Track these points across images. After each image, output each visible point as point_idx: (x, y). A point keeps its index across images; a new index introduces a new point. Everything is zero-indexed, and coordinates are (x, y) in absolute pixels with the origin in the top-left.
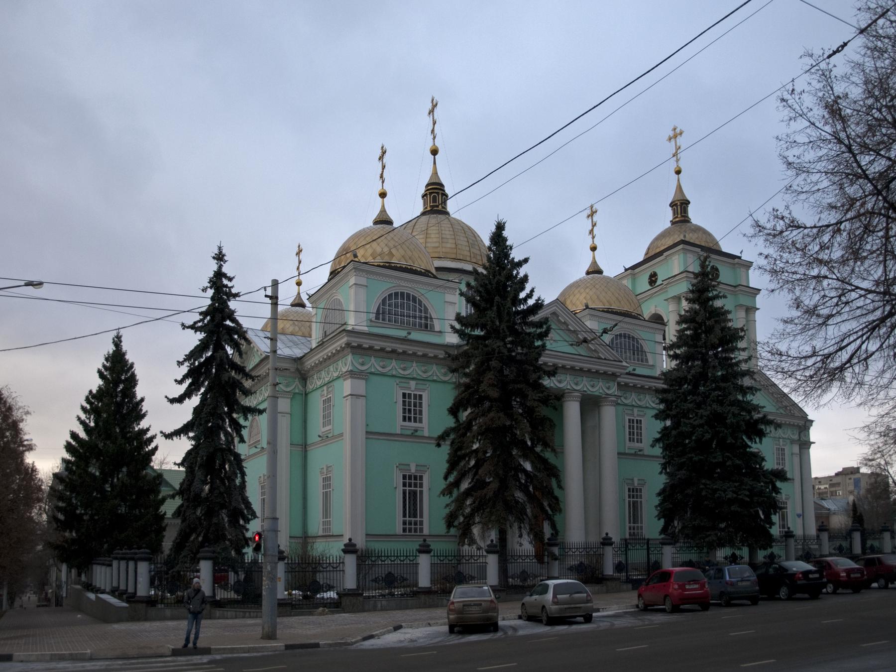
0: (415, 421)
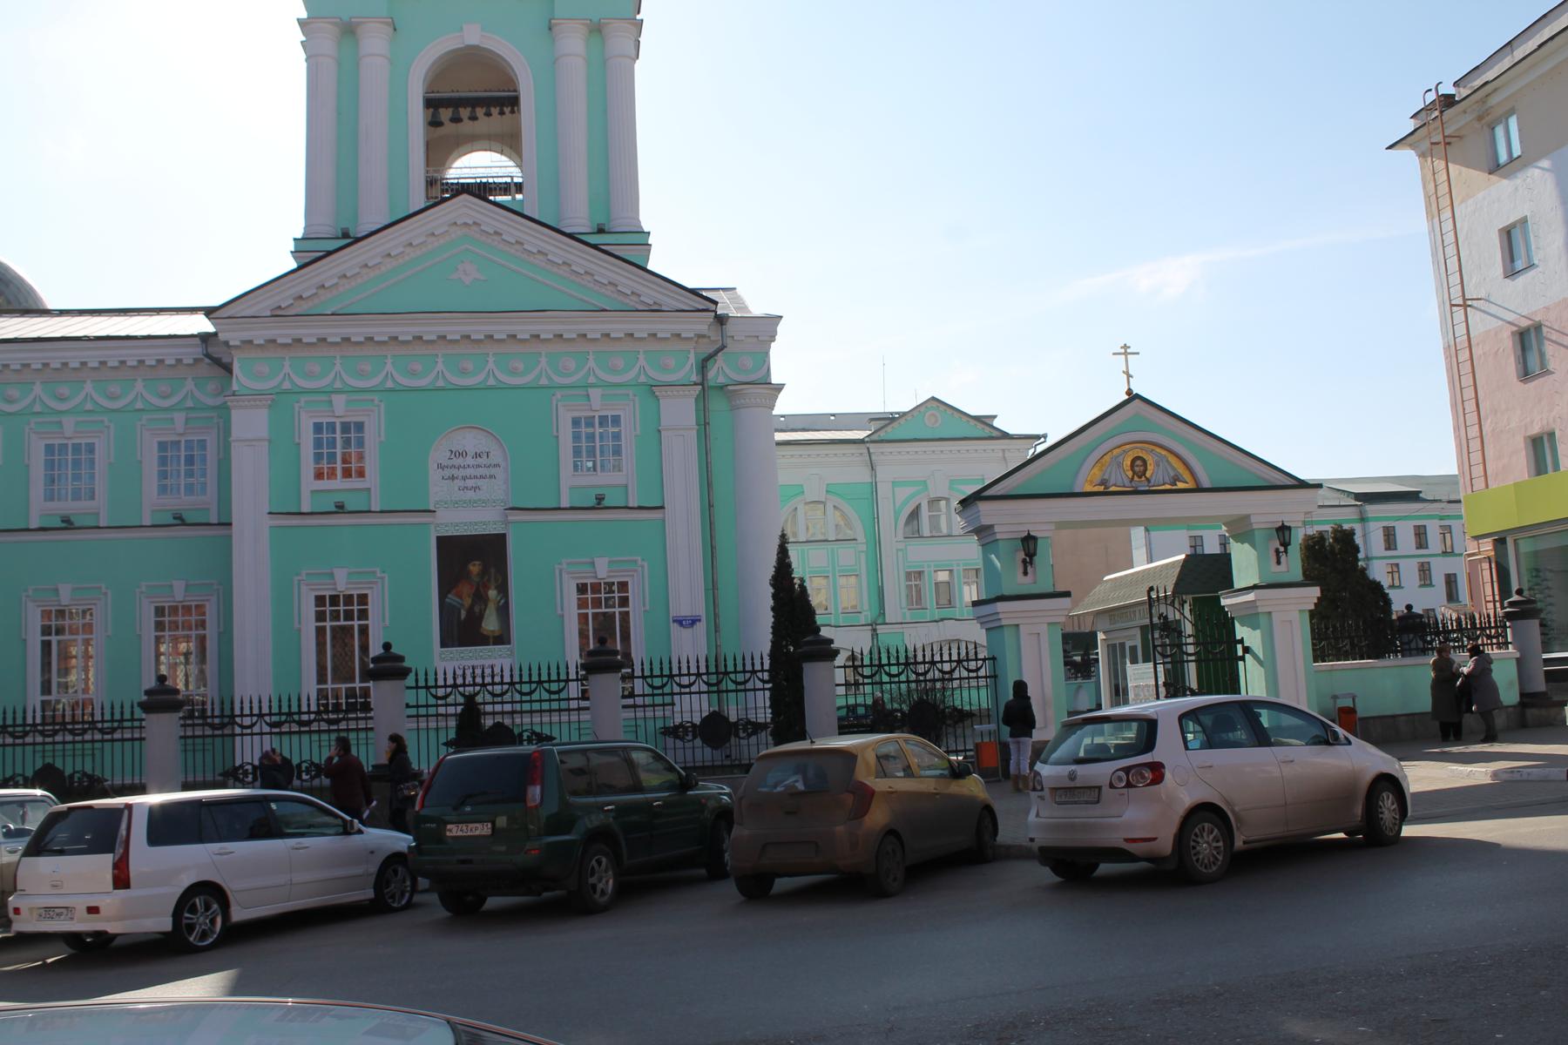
0: (347, 473)
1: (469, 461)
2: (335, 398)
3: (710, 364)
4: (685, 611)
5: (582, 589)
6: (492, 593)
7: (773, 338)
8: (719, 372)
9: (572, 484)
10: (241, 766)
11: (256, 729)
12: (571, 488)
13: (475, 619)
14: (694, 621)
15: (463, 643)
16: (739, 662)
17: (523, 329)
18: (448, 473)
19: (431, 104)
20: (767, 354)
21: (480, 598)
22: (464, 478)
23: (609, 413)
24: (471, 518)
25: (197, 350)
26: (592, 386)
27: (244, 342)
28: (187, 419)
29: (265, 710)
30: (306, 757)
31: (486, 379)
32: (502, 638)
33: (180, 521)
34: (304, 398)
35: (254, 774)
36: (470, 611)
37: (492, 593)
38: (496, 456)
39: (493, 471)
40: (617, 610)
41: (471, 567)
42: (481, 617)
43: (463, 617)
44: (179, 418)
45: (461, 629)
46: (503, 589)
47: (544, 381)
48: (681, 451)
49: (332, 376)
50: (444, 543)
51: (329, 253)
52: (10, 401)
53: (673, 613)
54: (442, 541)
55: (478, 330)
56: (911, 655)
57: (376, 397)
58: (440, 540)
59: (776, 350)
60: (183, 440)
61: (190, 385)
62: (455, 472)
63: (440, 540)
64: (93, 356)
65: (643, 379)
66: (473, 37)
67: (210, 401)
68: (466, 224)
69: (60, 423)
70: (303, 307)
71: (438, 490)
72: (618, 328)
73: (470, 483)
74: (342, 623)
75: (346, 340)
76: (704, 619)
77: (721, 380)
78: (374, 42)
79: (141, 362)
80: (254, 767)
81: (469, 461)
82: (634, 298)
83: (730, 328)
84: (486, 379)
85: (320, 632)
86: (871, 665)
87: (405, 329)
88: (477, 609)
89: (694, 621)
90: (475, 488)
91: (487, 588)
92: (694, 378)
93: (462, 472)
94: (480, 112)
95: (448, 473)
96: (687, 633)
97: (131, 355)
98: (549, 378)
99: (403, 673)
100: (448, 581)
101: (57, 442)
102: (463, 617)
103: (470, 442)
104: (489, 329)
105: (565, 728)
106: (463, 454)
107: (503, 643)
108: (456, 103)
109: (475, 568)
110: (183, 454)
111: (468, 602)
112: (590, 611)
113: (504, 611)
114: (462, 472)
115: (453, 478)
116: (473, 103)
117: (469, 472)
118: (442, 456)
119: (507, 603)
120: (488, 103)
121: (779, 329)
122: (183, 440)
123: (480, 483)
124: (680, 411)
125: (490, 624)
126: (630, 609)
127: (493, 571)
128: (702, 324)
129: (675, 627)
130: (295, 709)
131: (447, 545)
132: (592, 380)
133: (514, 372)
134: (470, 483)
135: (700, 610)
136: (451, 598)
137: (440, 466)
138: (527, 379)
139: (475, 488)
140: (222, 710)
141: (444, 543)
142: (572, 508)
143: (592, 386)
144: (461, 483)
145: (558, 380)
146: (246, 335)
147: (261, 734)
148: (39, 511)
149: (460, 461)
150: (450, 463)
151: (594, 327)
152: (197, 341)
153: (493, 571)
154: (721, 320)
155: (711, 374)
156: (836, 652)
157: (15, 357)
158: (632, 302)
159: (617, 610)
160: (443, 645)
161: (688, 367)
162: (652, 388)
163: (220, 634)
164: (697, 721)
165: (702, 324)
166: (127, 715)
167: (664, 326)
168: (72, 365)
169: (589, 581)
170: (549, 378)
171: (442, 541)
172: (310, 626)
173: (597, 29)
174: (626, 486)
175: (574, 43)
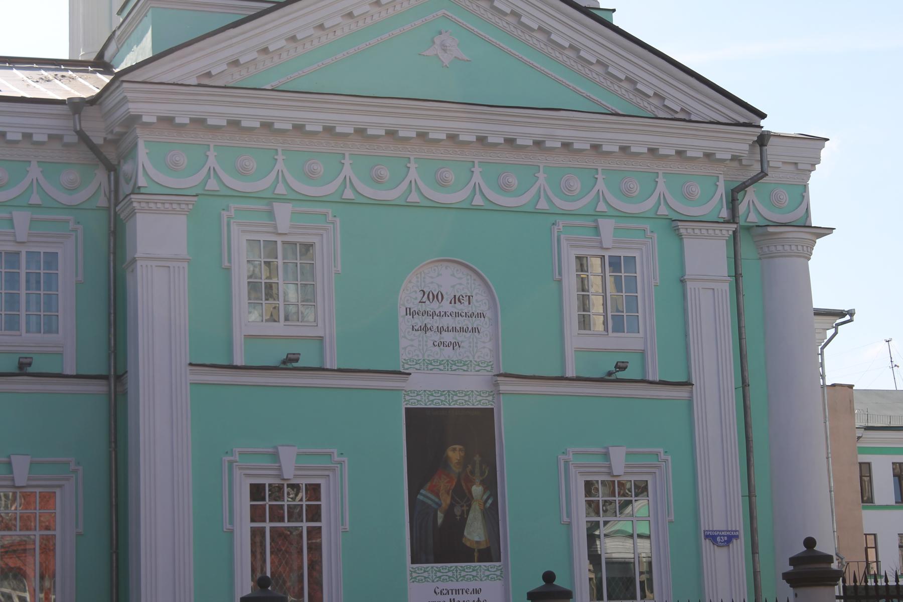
2: (278, 207)
3: (740, 196)
4: (718, 524)
5: (257, 491)
6: (477, 490)
8: (753, 208)
12: (578, 350)
14: (730, 538)
18: (418, 321)
20: (805, 187)
21: (462, 495)
22: (440, 330)
24: (457, 387)
26: (603, 215)
27: (194, 121)
31: (205, 182)
36: (449, 513)
37: (477, 490)
38: (480, 303)
41: (450, 453)
42: (462, 523)
44: (22, 218)
47: (543, 205)
48: (710, 308)
54: (412, 415)
58: (408, 410)
59: (817, 182)
60: (23, 250)
62: (428, 320)
65: (663, 210)
67: (64, 198)
70: (236, 77)
71: (410, 346)
72: (640, 138)
73: (448, 337)
74: (286, 524)
77: (753, 218)
79: (27, 136)
81: (446, 306)
82: (655, 101)
83: (771, 149)
84: (205, 182)
87: (696, 142)
88: (457, 511)
89: (730, 538)
90: (455, 345)
92: (725, 214)
93: (436, 322)
95: (418, 321)
96: (721, 553)
98: (549, 200)
99: (830, 578)
100: (419, 474)
102: (440, 521)
103: (450, 281)
106: (437, 297)
109: (454, 454)
110: (23, 271)
111: (446, 500)
112: (268, 525)
113: (492, 516)
114: (436, 322)
115: (425, 329)
117: (447, 322)
119: (495, 504)
121: (823, 153)
122: (23, 250)
124: (708, 255)
126: (323, 524)
128: (739, 143)
129: (706, 544)
132: (281, 190)
134: (448, 337)
135: (739, 524)
136: (424, 495)
137: (410, 312)
139: (455, 345)
142: (578, 379)
143: (603, 215)
144: (436, 337)
145: (369, 191)
149: (434, 306)
150: (422, 308)
151: (612, 137)
154: (763, 139)
155: (742, 208)
157: (13, 125)
158: (652, 106)
159: (305, 525)
161: (717, 198)
162: (675, 225)
163: (78, 535)
165: (739, 143)
167: (697, 143)
168: (36, 138)
169: (267, 481)
170: (549, 200)
174: (643, 353)
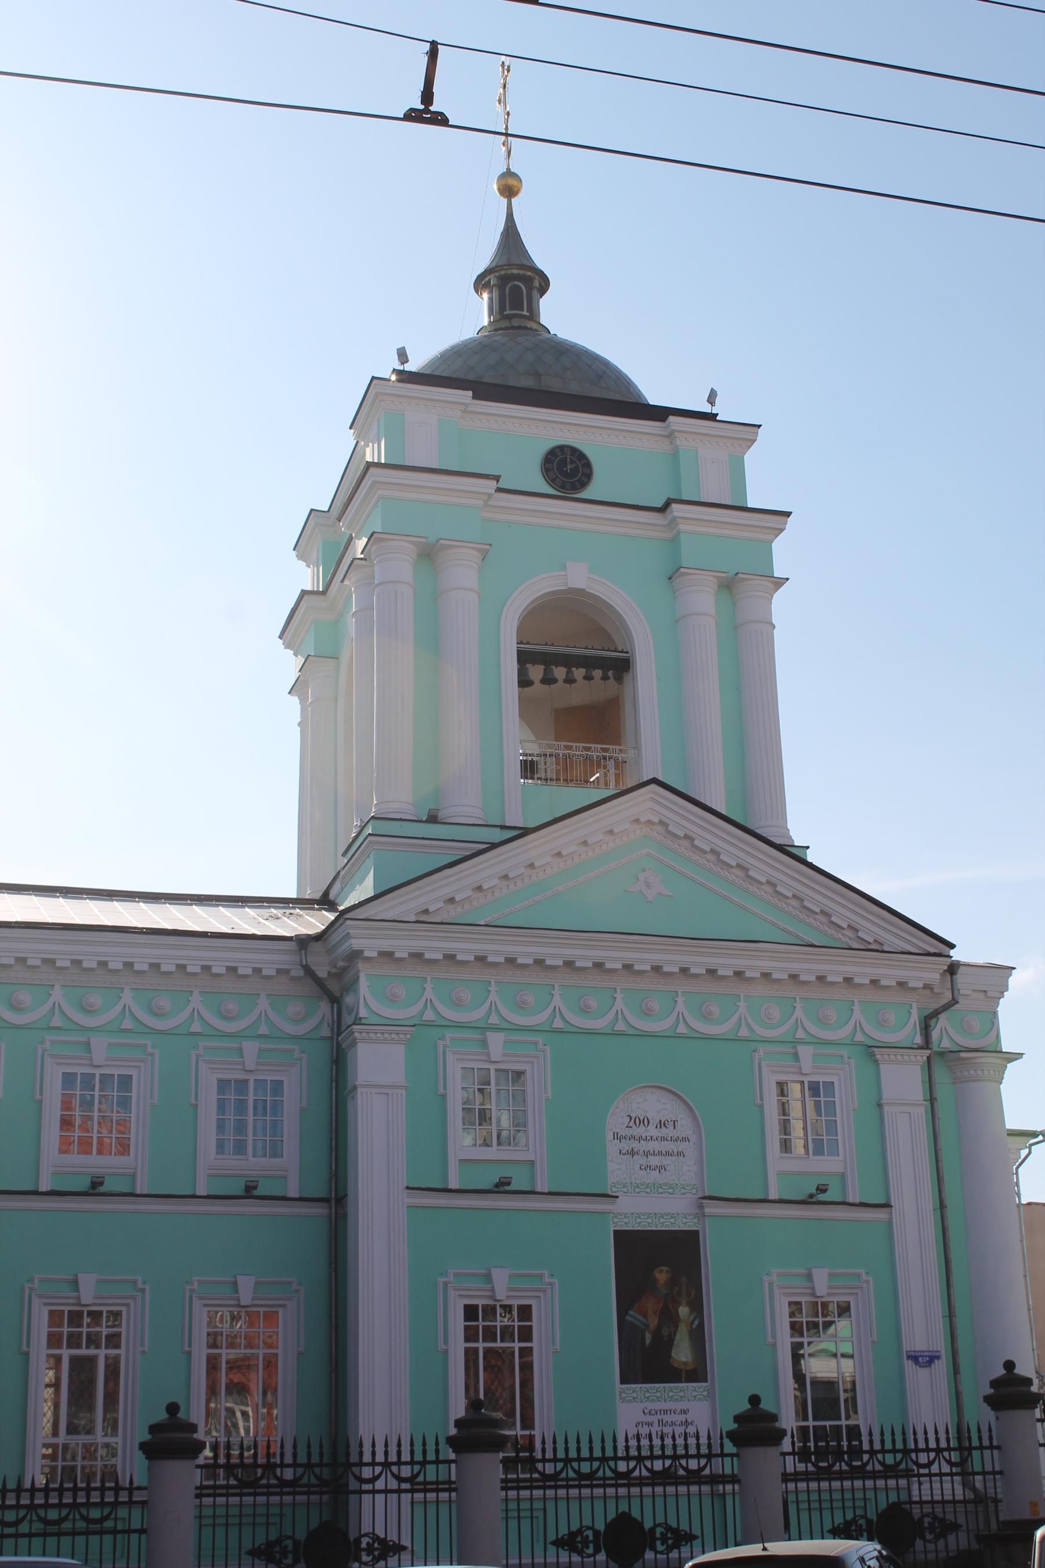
1: (652, 1131)
3: (933, 1022)
4: (920, 1345)
5: (470, 1312)
6: (683, 1311)
7: (1001, 994)
8: (947, 1032)
9: (785, 1170)
10: (580, 1531)
11: (380, 1485)
13: (664, 1344)
14: (932, 1359)
15: (649, 1377)
16: (549, 1446)
17: (726, 963)
18: (626, 1145)
19: (524, 658)
21: (669, 1317)
22: (646, 1154)
23: (821, 1079)
25: (286, 959)
26: (802, 1042)
27: (382, 954)
28: (260, 1050)
29: (393, 1458)
30: (660, 1519)
32: (697, 1373)
33: (249, 1192)
34: (450, 1033)
35: (654, 1539)
36: (657, 1334)
37: (683, 1311)
38: (685, 1127)
39: (682, 1146)
40: (517, 1345)
41: (658, 1275)
42: (670, 1343)
43: (648, 1341)
44: (251, 1048)
45: (648, 1360)
46: (697, 1305)
49: (611, 1015)
50: (624, 1240)
51: (494, 846)
52: (16, 1007)
53: (907, 1346)
54: (621, 1237)
55: (672, 960)
56: (276, 1449)
57: (540, 1039)
58: (615, 1232)
60: (252, 1078)
61: (263, 1004)
62: (635, 1145)
63: (615, 1232)
64: (142, 955)
65: (859, 1037)
66: (578, 578)
67: (290, 1028)
68: (649, 822)
69: (88, 1044)
70: (452, 913)
71: (618, 1170)
72: (836, 968)
73: (654, 1161)
74: (498, 1344)
75: (450, 958)
76: (943, 1356)
77: (946, 1044)
78: (463, 573)
80: (296, 1543)
81: (652, 1131)
83: (960, 977)
85: (470, 1355)
86: (294, 1465)
88: (665, 1332)
89: (932, 1359)
90: (661, 1168)
91: (678, 1304)
93: (643, 1146)
94: (579, 673)
95: (626, 1145)
96: (923, 1373)
97: (194, 957)
100: (629, 1293)
101: (80, 1070)
102: (648, 1341)
104: (685, 959)
105: (648, 1503)
106: (644, 1122)
107: (697, 1380)
108: (548, 660)
109: (662, 1276)
111: (653, 1321)
112: (481, 1345)
113: (698, 1337)
114: (643, 1146)
115: (632, 1153)
116: (569, 661)
118: (617, 1122)
119: (701, 1325)
120: (589, 663)
123: (666, 1161)
124: (903, 1080)
125: (682, 1353)
127: (684, 1279)
128: (931, 972)
129: (909, 1364)
130: (393, 1458)
131: (628, 1243)
132: (494, 1019)
133: (457, 1003)
134: (654, 1161)
135: (941, 1345)
136: (632, 1315)
137: (617, 1136)
138: (540, 1019)
139: (661, 1168)
140: (295, 1455)
141: (624, 1240)
143: (802, 1042)
146: (385, 945)
147: (386, 1491)
148: (55, 1163)
149: (639, 1131)
150: (629, 1132)
151: (808, 967)
152: (293, 945)
153: (684, 1279)
154: (953, 968)
155: (935, 1034)
156: (201, 1446)
158: (846, 938)
160: (623, 1381)
162: (871, 1051)
163: (300, 1353)
164: (301, 1535)
165: (931, 972)
166: (431, 1456)
167: (890, 972)
169: (480, 1302)
171: (621, 1237)
172: (458, 1346)
173: (729, 585)
174: (843, 1175)
175: (703, 599)
